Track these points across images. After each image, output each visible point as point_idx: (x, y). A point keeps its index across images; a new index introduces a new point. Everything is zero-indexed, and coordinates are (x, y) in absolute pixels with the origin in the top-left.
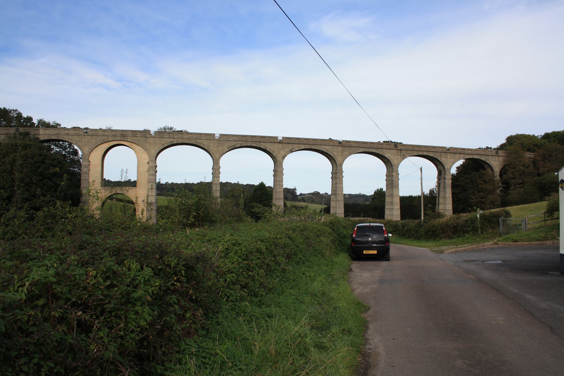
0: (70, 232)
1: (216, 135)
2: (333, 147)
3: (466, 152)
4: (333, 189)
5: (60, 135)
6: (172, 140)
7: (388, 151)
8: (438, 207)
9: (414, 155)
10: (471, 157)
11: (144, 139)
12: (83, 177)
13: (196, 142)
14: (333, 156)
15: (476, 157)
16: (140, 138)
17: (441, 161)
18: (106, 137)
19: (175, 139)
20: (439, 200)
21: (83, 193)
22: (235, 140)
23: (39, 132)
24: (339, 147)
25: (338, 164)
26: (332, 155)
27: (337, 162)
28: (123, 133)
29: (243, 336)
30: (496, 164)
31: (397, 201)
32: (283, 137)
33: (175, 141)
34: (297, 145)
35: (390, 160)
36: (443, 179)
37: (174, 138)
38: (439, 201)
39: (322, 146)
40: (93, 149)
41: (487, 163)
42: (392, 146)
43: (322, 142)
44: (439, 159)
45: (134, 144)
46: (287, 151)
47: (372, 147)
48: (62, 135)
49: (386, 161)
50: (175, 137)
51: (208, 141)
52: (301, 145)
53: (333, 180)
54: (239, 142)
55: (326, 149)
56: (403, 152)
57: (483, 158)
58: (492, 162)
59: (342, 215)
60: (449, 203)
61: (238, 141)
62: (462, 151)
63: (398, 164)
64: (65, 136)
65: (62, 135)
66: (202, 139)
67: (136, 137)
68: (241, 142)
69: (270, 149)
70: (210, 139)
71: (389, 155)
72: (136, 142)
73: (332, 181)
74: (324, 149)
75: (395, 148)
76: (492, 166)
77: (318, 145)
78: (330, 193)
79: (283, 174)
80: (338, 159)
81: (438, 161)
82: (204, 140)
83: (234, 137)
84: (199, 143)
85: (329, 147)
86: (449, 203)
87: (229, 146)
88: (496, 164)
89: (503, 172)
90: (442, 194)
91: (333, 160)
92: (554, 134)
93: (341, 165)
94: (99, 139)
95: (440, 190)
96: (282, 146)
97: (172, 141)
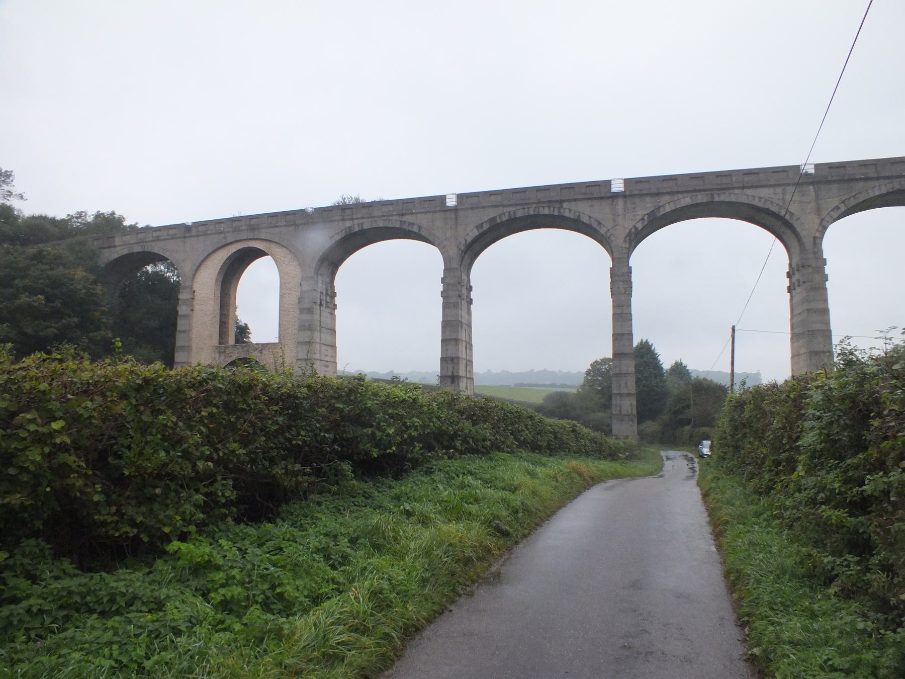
1: (613, 182)
2: (783, 190)
4: (795, 320)
5: (146, 242)
6: (348, 224)
11: (292, 228)
12: (181, 324)
13: (401, 222)
16: (284, 229)
18: (222, 236)
19: (356, 222)
21: (175, 361)
22: (669, 190)
23: (114, 241)
25: (805, 240)
27: (803, 234)
28: (253, 222)
32: (625, 180)
33: (356, 226)
34: (667, 198)
37: (352, 219)
40: (200, 265)
43: (746, 178)
45: (274, 244)
46: (640, 218)
47: (894, 174)
48: (149, 242)
50: (354, 217)
51: (430, 216)
52: (680, 196)
54: (507, 210)
55: (760, 198)
61: (504, 206)
64: (154, 244)
65: (149, 242)
66: (416, 213)
67: (277, 227)
68: (511, 209)
69: (590, 217)
70: (433, 210)
72: (277, 240)
73: (791, 300)
74: (757, 200)
77: (734, 188)
78: (277, 341)
79: (826, 278)
80: (806, 224)
82: (419, 216)
83: (493, 198)
84: (410, 224)
85: (771, 190)
87: (480, 222)
93: (817, 242)
94: (643, 209)
96: (625, 203)
97: (350, 228)
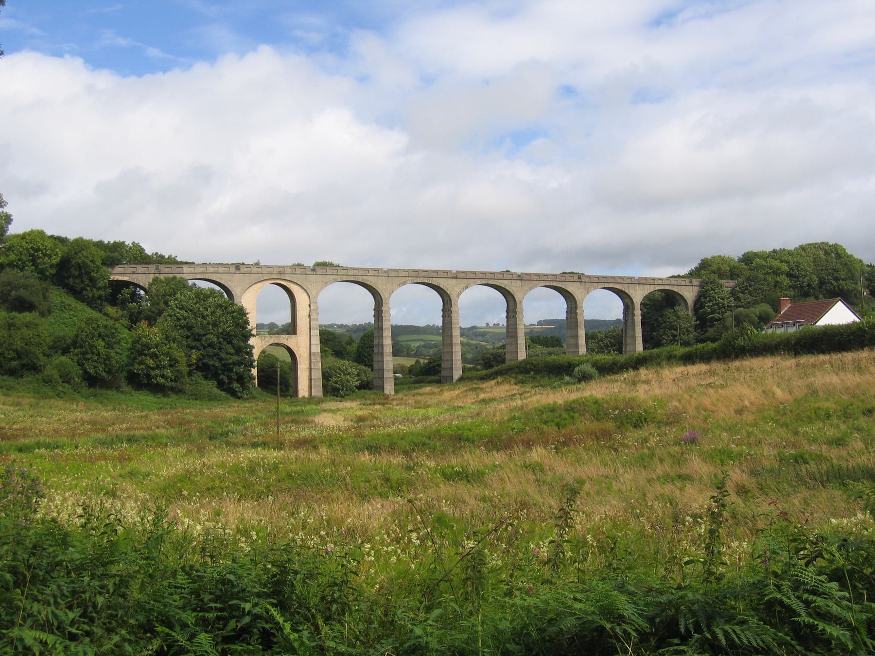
0: (254, 469)
3: (656, 282)
7: (571, 283)
8: (626, 348)
9: (483, 283)
10: (662, 287)
14: (512, 292)
15: (667, 288)
17: (630, 294)
20: (626, 340)
24: (518, 281)
26: (511, 291)
29: (575, 617)
30: (689, 294)
31: (648, 352)
35: (445, 289)
36: (630, 315)
38: (626, 342)
39: (500, 281)
41: (680, 295)
42: (576, 277)
44: (627, 291)
49: (624, 296)
50: (339, 274)
53: (446, 313)
56: (588, 285)
57: (675, 289)
58: (685, 293)
59: (373, 322)
60: (639, 344)
62: (652, 282)
63: (583, 299)
71: (573, 288)
75: (578, 280)
76: (686, 298)
81: (626, 293)
86: (639, 344)
88: (689, 294)
89: (699, 303)
90: (629, 333)
91: (510, 296)
92: (827, 253)
95: (628, 328)
